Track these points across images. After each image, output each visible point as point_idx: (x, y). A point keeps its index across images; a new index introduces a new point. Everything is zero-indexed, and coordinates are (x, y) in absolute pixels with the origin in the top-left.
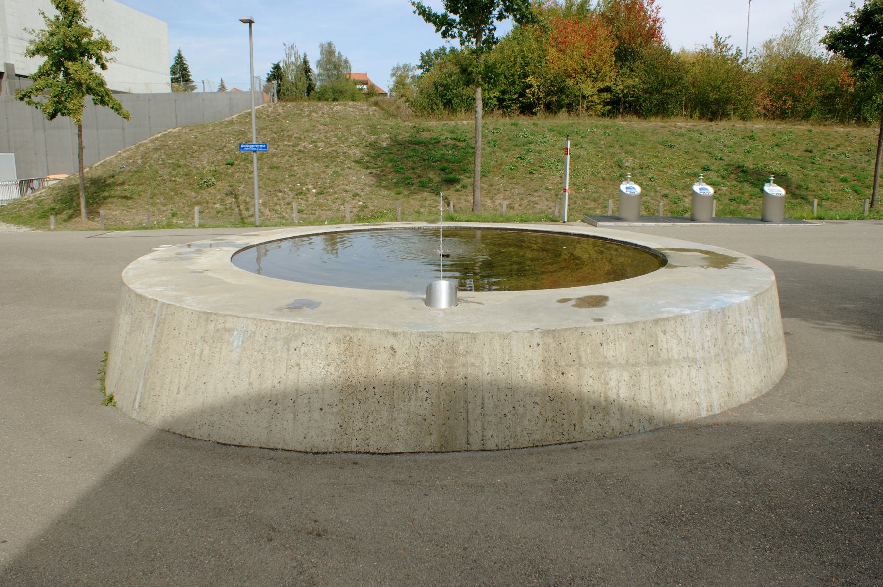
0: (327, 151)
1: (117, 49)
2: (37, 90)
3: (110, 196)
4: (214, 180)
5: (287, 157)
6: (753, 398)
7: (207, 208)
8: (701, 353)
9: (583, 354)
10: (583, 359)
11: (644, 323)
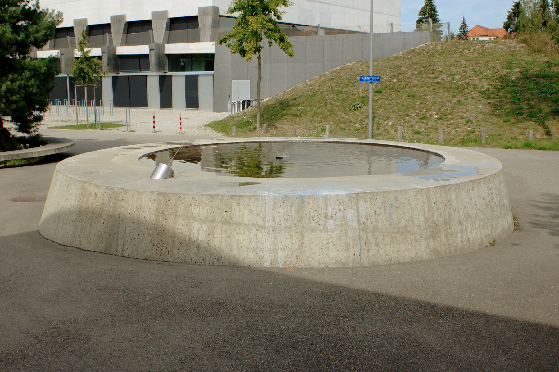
0: (460, 83)
1: (292, 4)
2: (230, 37)
3: (287, 114)
4: (361, 104)
5: (425, 88)
6: (330, 266)
7: (349, 126)
8: (271, 223)
9: (179, 209)
10: (179, 212)
11: (223, 196)
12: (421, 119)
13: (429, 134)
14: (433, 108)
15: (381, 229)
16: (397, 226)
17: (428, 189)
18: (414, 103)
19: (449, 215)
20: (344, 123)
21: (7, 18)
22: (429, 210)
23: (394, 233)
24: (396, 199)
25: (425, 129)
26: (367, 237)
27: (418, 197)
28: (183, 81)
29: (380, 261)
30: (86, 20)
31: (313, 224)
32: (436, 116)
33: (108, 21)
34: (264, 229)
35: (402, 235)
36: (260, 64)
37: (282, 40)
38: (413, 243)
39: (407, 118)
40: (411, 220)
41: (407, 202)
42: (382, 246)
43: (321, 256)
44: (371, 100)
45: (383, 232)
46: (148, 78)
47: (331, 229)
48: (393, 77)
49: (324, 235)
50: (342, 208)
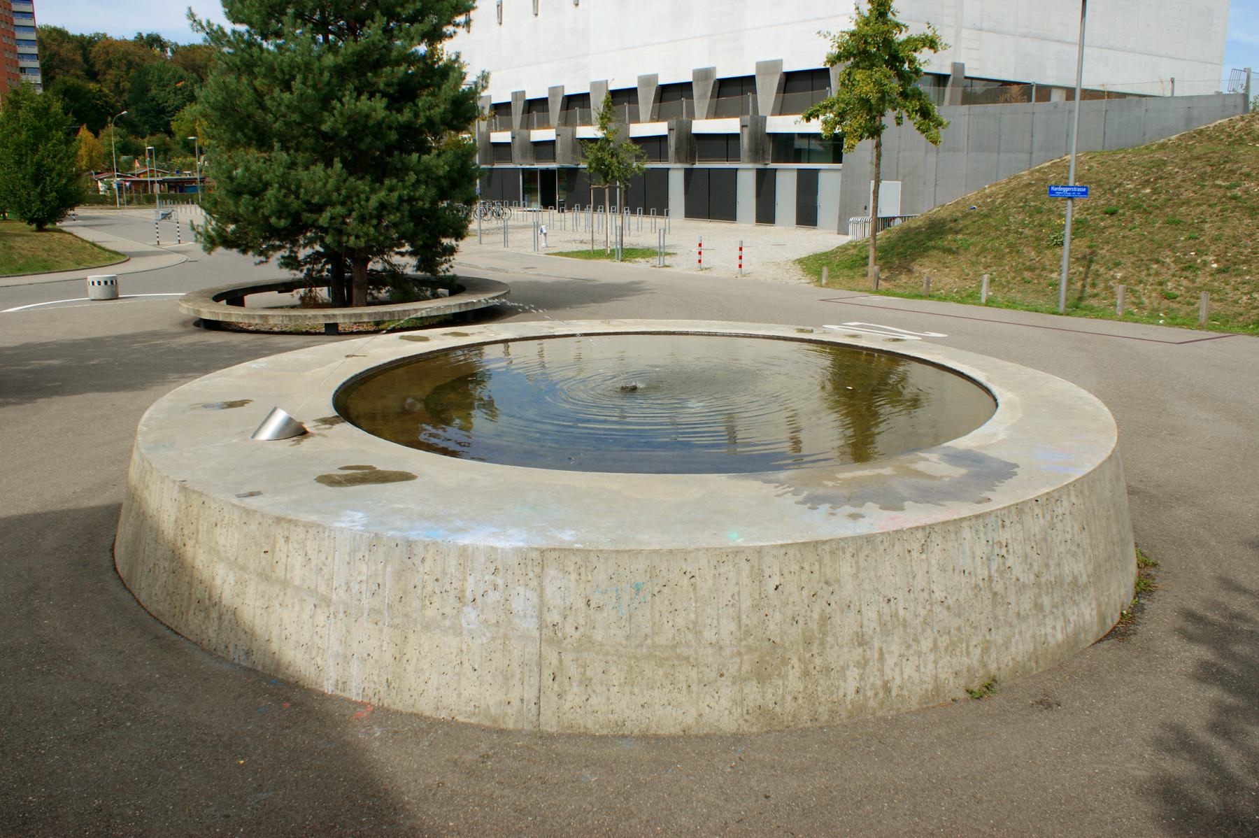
1: (946, 46)
3: (934, 248)
5: (1205, 207)
6: (460, 719)
8: (341, 592)
12: (1183, 270)
13: (1192, 300)
14: (1213, 247)
15: (601, 644)
16: (649, 641)
17: (759, 551)
18: (1176, 237)
19: (825, 620)
20: (1031, 269)
21: (382, 86)
22: (756, 607)
23: (637, 659)
24: (652, 572)
25: (1188, 290)
26: (561, 661)
27: (723, 569)
28: (793, 177)
29: (590, 725)
30: (656, 77)
31: (430, 612)
32: (1215, 266)
33: (689, 78)
34: (328, 606)
35: (660, 665)
36: (879, 156)
37: (925, 113)
38: (694, 688)
39: (1155, 266)
40: (695, 629)
41: (685, 581)
42: (598, 689)
43: (442, 691)
44: (1068, 232)
45: (607, 653)
46: (739, 173)
47: (470, 631)
48: (1146, 183)
49: (452, 642)
50: (500, 582)
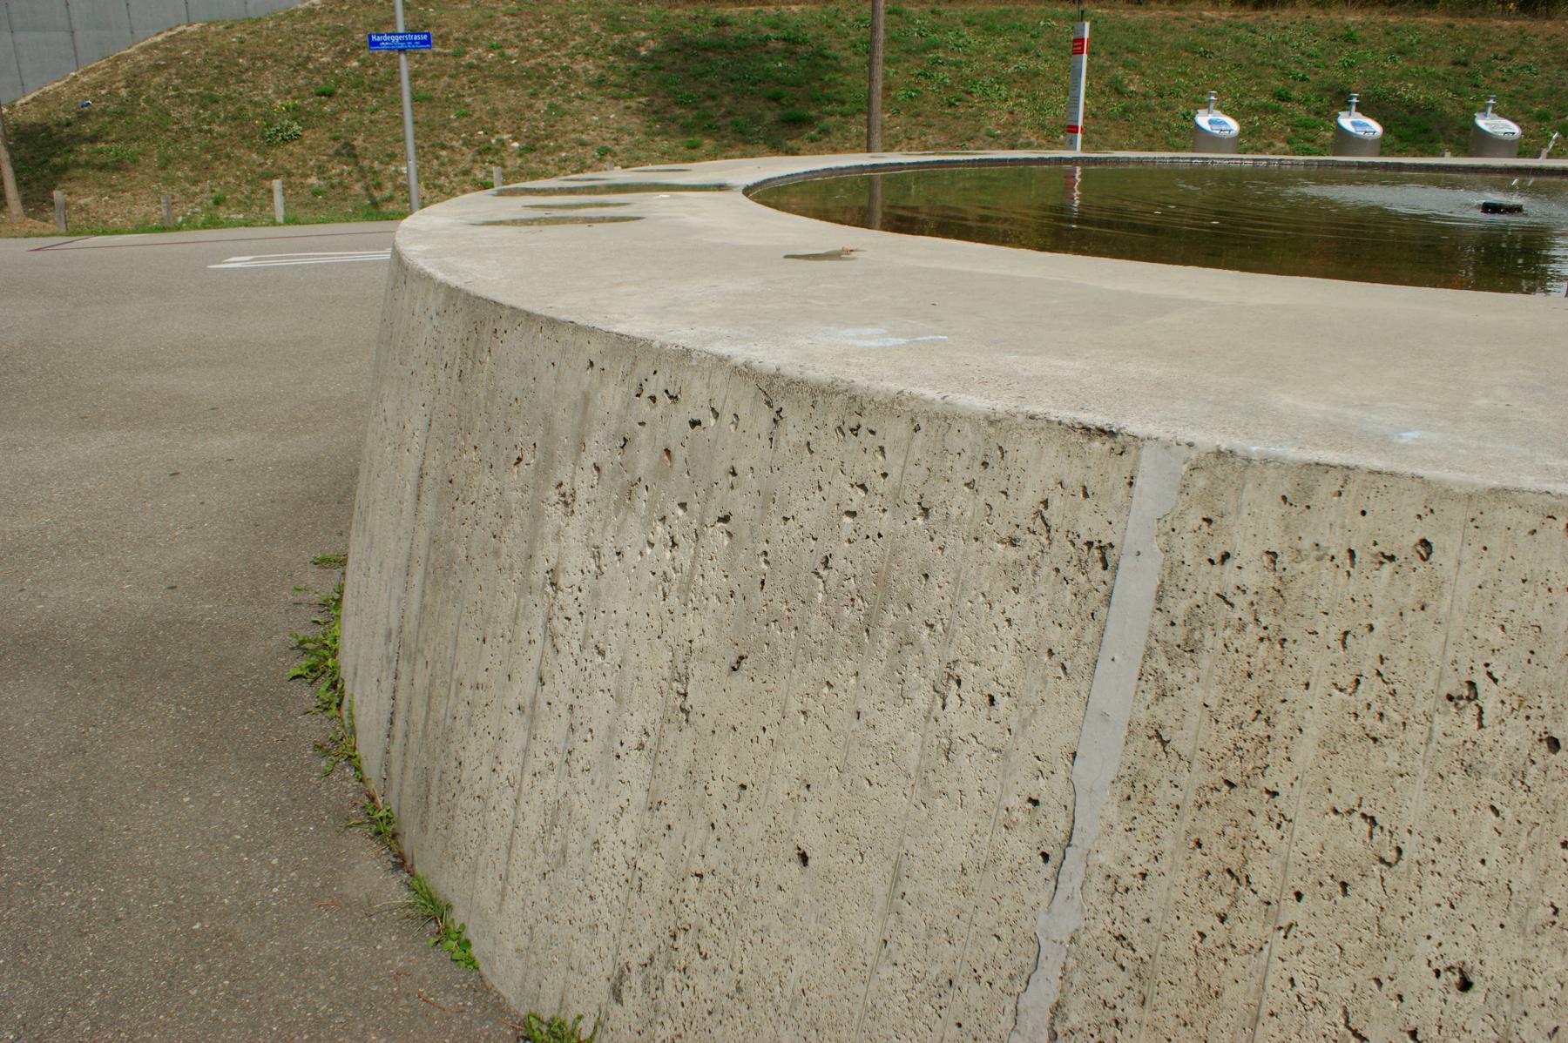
0: (528, 64)
32: (516, 144)
39: (444, 153)
